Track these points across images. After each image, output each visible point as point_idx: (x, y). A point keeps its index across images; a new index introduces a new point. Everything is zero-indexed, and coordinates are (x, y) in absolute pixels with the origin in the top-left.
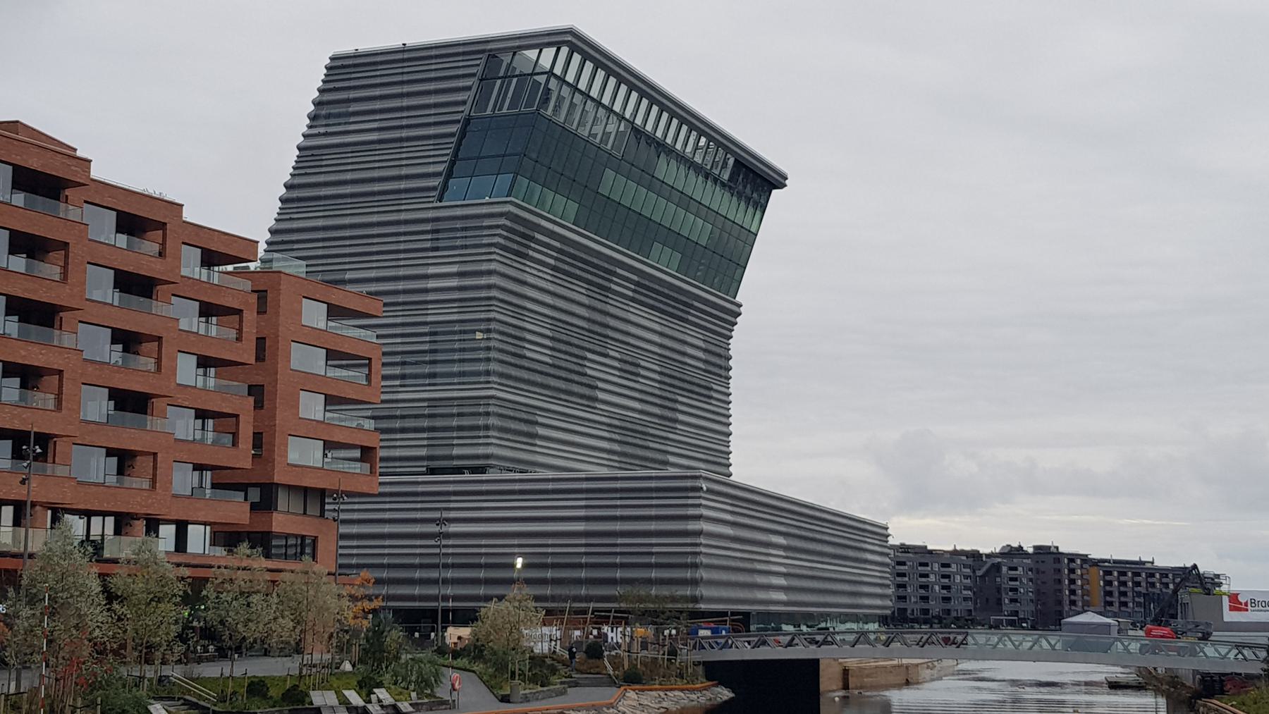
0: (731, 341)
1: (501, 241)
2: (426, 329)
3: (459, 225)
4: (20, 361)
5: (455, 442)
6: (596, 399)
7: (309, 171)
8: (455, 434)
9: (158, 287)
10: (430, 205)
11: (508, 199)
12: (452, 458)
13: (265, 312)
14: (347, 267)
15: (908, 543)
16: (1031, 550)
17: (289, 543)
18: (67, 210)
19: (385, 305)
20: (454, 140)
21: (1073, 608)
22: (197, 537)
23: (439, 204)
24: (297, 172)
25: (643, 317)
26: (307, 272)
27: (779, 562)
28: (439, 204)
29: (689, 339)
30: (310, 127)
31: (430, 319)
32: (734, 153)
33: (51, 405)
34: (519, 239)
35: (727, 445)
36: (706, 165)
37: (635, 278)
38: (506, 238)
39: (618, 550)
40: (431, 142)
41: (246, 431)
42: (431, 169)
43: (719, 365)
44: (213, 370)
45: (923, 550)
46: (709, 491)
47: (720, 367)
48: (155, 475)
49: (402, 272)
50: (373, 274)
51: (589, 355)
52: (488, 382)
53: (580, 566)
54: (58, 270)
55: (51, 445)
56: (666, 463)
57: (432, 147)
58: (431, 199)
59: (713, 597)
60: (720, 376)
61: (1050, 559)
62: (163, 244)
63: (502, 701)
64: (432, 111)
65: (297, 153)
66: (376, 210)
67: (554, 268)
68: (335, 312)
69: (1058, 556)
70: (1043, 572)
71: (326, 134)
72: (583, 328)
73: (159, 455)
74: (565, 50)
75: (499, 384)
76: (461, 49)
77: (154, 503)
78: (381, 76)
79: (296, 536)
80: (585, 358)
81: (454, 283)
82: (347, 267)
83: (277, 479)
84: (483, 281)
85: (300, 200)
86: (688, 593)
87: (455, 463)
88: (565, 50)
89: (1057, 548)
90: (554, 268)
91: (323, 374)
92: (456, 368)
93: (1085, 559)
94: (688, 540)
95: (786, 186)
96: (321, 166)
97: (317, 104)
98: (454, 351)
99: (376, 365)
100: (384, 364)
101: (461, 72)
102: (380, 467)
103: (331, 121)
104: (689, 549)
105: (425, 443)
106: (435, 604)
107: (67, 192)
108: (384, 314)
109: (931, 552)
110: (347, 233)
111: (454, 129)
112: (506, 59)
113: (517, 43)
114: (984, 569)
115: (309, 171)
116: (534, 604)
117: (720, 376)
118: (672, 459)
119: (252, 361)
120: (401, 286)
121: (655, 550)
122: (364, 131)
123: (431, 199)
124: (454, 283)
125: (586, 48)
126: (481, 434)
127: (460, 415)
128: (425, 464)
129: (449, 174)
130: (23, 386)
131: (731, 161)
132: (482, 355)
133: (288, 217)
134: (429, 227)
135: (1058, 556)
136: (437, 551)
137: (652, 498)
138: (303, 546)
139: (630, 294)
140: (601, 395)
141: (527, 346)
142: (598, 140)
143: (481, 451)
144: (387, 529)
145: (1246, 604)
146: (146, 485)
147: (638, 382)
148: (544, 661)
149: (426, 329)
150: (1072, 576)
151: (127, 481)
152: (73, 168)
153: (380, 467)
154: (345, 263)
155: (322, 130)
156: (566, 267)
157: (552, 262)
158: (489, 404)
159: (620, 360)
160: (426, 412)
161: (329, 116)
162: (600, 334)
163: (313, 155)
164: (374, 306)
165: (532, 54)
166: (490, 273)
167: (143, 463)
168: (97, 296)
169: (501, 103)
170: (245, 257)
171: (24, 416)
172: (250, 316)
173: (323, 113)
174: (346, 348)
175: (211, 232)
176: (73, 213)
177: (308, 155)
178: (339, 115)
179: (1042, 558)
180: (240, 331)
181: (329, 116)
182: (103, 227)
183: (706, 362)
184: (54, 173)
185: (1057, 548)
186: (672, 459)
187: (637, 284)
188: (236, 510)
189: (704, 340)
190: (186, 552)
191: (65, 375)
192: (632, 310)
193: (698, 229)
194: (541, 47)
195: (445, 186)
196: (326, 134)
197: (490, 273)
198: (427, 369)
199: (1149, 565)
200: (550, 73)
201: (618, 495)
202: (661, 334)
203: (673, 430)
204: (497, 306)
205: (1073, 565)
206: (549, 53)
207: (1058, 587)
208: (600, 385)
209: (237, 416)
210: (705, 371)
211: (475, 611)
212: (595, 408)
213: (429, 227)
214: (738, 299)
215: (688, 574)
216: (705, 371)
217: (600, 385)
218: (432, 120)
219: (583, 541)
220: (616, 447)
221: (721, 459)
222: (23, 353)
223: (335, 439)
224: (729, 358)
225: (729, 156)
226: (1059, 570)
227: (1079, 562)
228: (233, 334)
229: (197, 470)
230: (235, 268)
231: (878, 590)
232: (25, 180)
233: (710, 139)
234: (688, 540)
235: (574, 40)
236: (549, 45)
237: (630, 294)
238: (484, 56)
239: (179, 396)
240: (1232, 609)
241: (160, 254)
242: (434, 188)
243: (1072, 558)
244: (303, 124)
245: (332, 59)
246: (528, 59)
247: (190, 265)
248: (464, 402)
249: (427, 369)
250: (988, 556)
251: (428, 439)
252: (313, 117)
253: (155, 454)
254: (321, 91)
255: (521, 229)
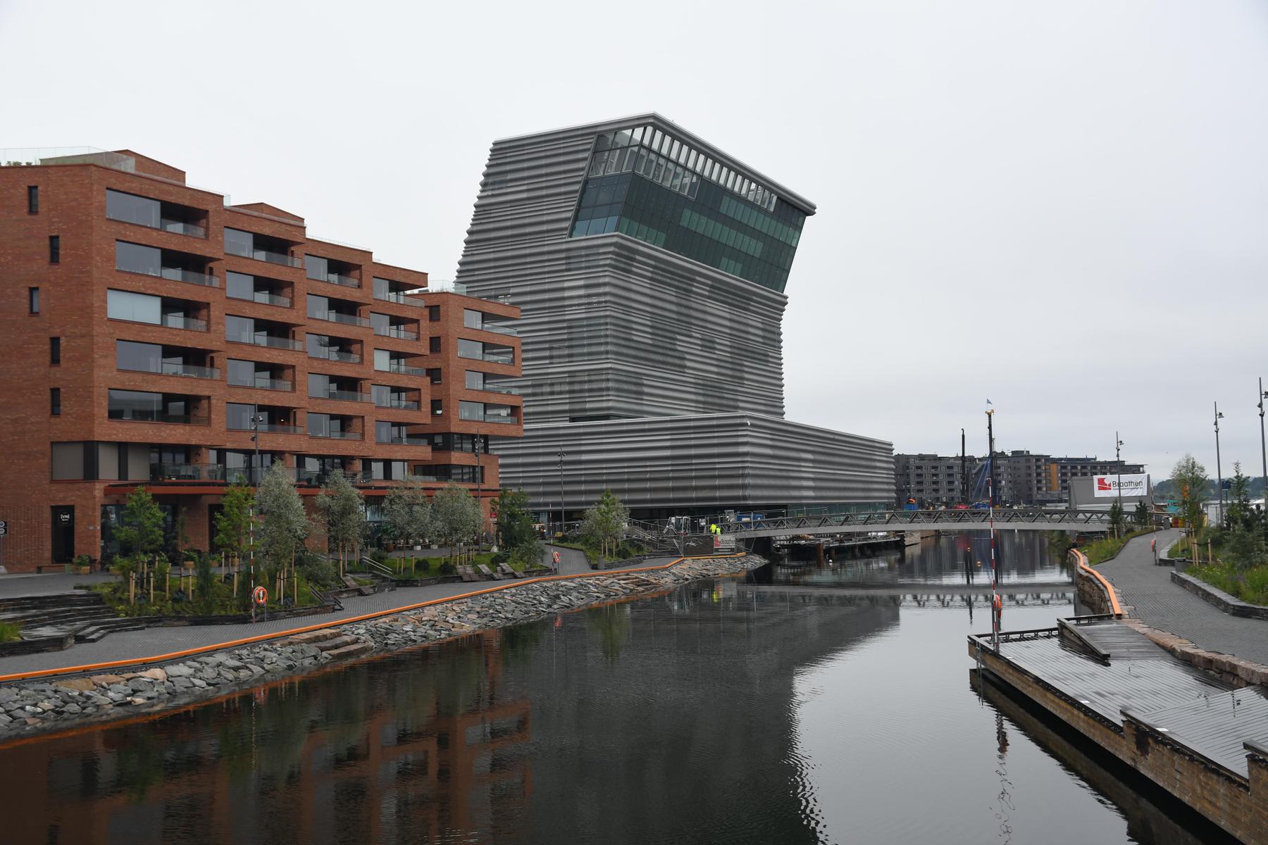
0: (781, 322)
1: (613, 262)
2: (565, 325)
3: (583, 253)
4: (266, 361)
5: (587, 400)
6: (685, 367)
7: (482, 221)
8: (587, 395)
9: (360, 308)
10: (564, 240)
11: (616, 233)
12: (586, 410)
13: (439, 320)
14: (511, 285)
15: (925, 453)
16: (1010, 455)
17: (464, 471)
18: (293, 261)
19: (522, 311)
20: (578, 195)
21: (1040, 492)
22: (398, 470)
23: (570, 239)
24: (475, 222)
25: (595, 277)
26: (467, 292)
27: (808, 470)
28: (570, 239)
29: (751, 322)
30: (482, 191)
31: (567, 317)
32: (776, 193)
33: (289, 388)
34: (624, 260)
35: (781, 392)
36: (757, 202)
37: (710, 282)
38: (615, 260)
39: (693, 467)
40: (563, 197)
41: (426, 399)
42: (563, 216)
43: (773, 338)
44: (403, 360)
45: (935, 458)
46: (752, 425)
47: (774, 340)
48: (363, 431)
49: (547, 287)
50: (528, 289)
51: (679, 337)
52: (608, 359)
53: (668, 479)
54: (288, 300)
55: (292, 415)
56: (737, 408)
57: (563, 201)
58: (564, 236)
59: (756, 496)
60: (775, 347)
61: (1023, 460)
62: (360, 280)
63: (593, 569)
64: (544, 179)
65: (474, 209)
66: (510, 248)
67: (651, 279)
68: (486, 317)
69: (1029, 458)
70: (1019, 469)
71: (493, 196)
72: (674, 319)
73: (366, 418)
74: (650, 129)
75: (615, 359)
76: (580, 132)
77: (363, 449)
78: (527, 154)
79: (469, 466)
80: (676, 339)
81: (582, 292)
82: (511, 285)
83: (453, 430)
84: (601, 290)
85: (477, 241)
86: (626, 498)
87: (588, 414)
88: (650, 129)
89: (1028, 452)
90: (651, 279)
91: (481, 358)
92: (585, 350)
93: (1047, 458)
94: (740, 459)
95: (815, 213)
96: (491, 218)
97: (486, 175)
98: (583, 338)
99: (518, 352)
100: (524, 351)
101: (580, 148)
102: (524, 420)
103: (496, 187)
104: (740, 465)
105: (568, 401)
106: (560, 508)
107: (292, 248)
108: (522, 317)
109: (940, 458)
110: (510, 262)
111: (577, 187)
112: (611, 137)
113: (617, 126)
114: (977, 469)
115: (482, 221)
116: (623, 506)
117: (775, 347)
118: (741, 405)
119: (428, 352)
120: (546, 296)
121: (717, 466)
122: (517, 192)
123: (564, 236)
124: (582, 292)
125: (665, 127)
126: (604, 393)
127: (590, 381)
128: (568, 415)
129: (576, 218)
130: (272, 377)
131: (775, 198)
132: (602, 340)
133: (470, 253)
134: (563, 255)
135: (1029, 458)
136: (560, 473)
137: (714, 432)
138: (474, 472)
139: (707, 293)
140: (688, 364)
141: (634, 332)
142: (677, 190)
143: (604, 405)
144: (541, 459)
145: (1110, 485)
146: (359, 437)
147: (714, 353)
148: (633, 542)
149: (565, 325)
150: (1039, 471)
151: (348, 435)
152: (294, 233)
153: (524, 420)
154: (509, 283)
155: (490, 193)
156: (660, 278)
157: (649, 274)
158: (608, 373)
159: (730, 347)
160: (567, 380)
161: (494, 183)
162: (685, 321)
163: (484, 211)
164: (514, 312)
165: (628, 132)
166: (605, 284)
167: (356, 423)
168: (319, 315)
169: (612, 166)
170: (419, 284)
171: (271, 396)
172: (425, 323)
173: (492, 180)
174: (497, 341)
175: (395, 269)
176: (297, 263)
177: (482, 210)
178: (501, 182)
179: (1018, 459)
180: (418, 333)
181: (494, 183)
182: (319, 270)
183: (678, 313)
184: (281, 237)
185: (1028, 452)
186: (741, 405)
187: (711, 286)
188: (423, 452)
189: (676, 296)
190: (391, 479)
191: (297, 369)
192: (708, 304)
193: (755, 248)
194: (633, 128)
195: (573, 228)
196: (493, 196)
197: (605, 284)
198: (547, 353)
199: (1093, 461)
200: (641, 145)
201: (692, 431)
202: (730, 320)
203: (742, 385)
204: (611, 307)
205: (1039, 463)
206: (639, 132)
207: (1029, 478)
208: (688, 356)
209: (420, 390)
210: (763, 343)
211: (581, 511)
212: (685, 373)
213: (563, 255)
214: (785, 293)
215: (740, 481)
216: (763, 343)
217: (688, 356)
218: (544, 185)
219: (670, 463)
220: (701, 398)
221: (775, 404)
222: (268, 356)
223: (492, 402)
224: (781, 334)
225: (773, 195)
226: (1029, 467)
227: (1043, 461)
228: (414, 335)
229: (395, 426)
230: (420, 291)
231: (886, 487)
232: (261, 242)
233: (758, 184)
234: (740, 459)
235: (656, 122)
236: (639, 126)
237: (707, 293)
238: (595, 136)
239: (379, 378)
240: (1100, 488)
241: (359, 287)
242: (565, 229)
243: (1038, 458)
244: (477, 190)
245: (495, 144)
246: (626, 136)
247: (382, 292)
248: (592, 373)
249: (566, 352)
250: (980, 459)
251: (570, 398)
252: (484, 185)
253: (363, 417)
254: (488, 166)
255: (625, 253)
